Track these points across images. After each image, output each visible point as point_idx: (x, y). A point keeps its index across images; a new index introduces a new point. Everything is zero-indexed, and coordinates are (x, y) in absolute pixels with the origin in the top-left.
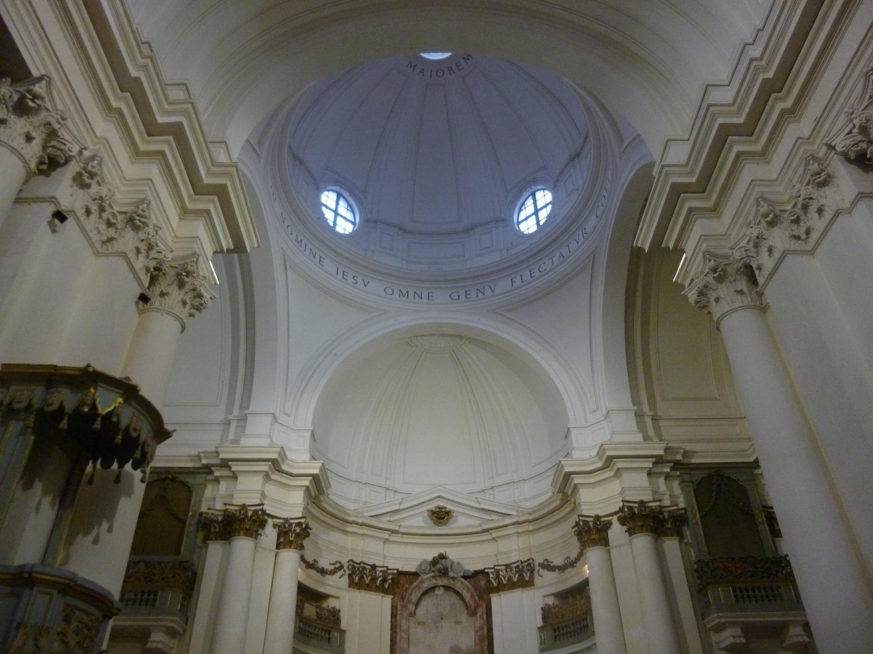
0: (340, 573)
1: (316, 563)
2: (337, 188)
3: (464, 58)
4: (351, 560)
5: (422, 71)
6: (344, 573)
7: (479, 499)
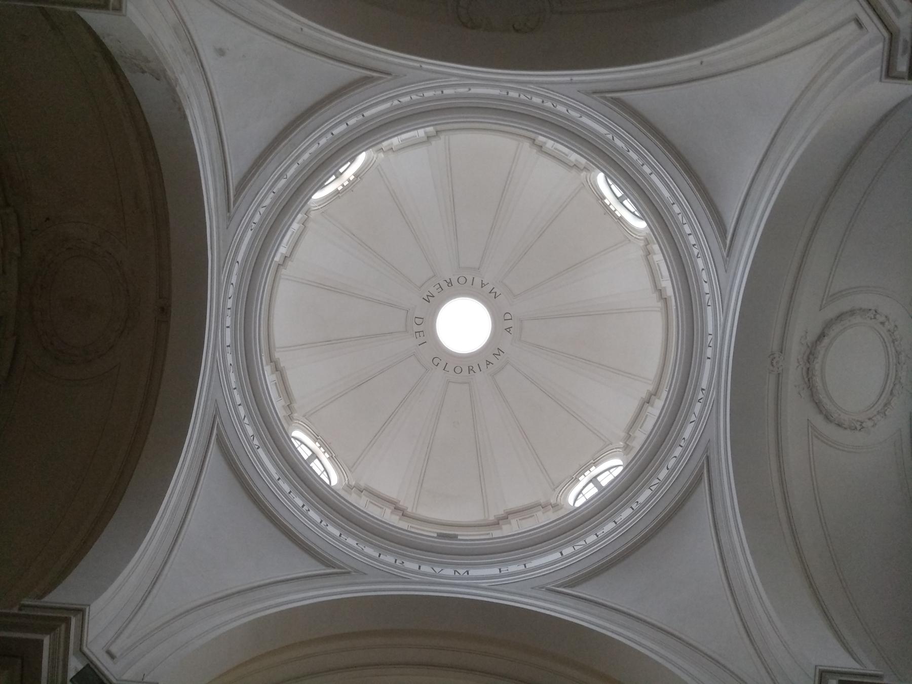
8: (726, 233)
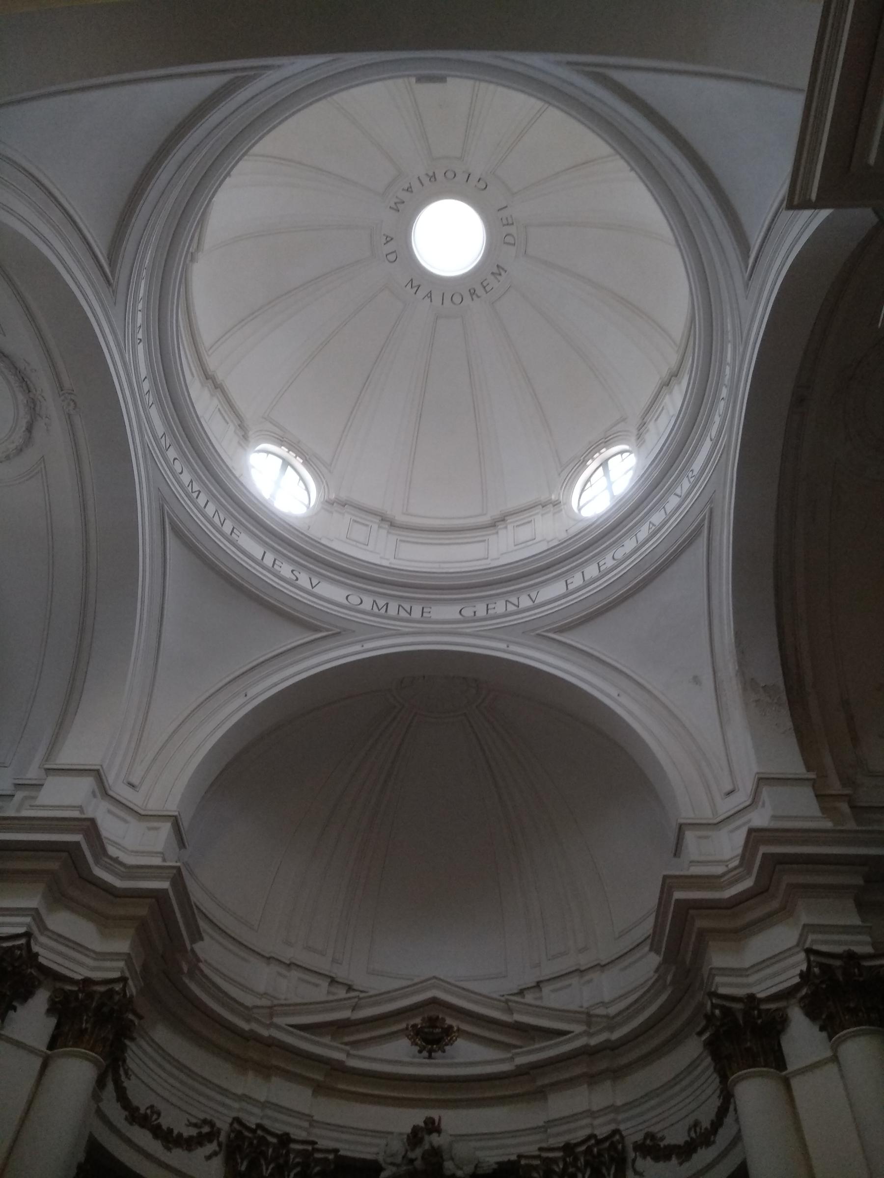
0: (212, 1147)
1: (155, 1117)
2: (283, 451)
3: (493, 273)
4: (237, 1120)
5: (430, 295)
6: (217, 1149)
7: (510, 1004)
8: (172, 529)
